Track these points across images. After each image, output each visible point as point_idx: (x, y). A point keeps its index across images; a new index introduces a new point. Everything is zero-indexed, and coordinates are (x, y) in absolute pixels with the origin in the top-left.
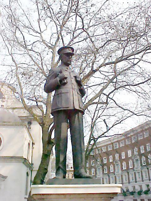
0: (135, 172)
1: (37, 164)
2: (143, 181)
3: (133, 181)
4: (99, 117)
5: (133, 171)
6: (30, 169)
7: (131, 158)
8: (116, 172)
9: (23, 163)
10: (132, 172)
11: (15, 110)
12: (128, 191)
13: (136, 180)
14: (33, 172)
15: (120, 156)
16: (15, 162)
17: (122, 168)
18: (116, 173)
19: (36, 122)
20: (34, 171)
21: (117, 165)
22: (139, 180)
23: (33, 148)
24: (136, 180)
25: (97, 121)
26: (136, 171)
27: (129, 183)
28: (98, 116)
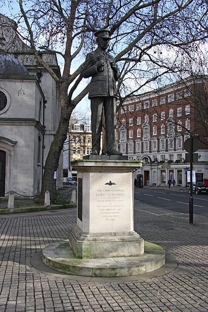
1: (125, 61)
2: (175, 150)
3: (180, 148)
4: (130, 70)
5: (164, 137)
6: (42, 133)
7: (140, 126)
8: (120, 141)
9: (35, 126)
10: (138, 142)
11: (20, 57)
12: (156, 160)
13: (142, 150)
14: (45, 136)
15: (151, 119)
17: (128, 136)
18: (120, 142)
19: (48, 74)
20: (47, 134)
21: (123, 132)
22: (178, 148)
23: (45, 107)
24: (142, 150)
25: (126, 76)
27: (158, 151)
28: (128, 70)
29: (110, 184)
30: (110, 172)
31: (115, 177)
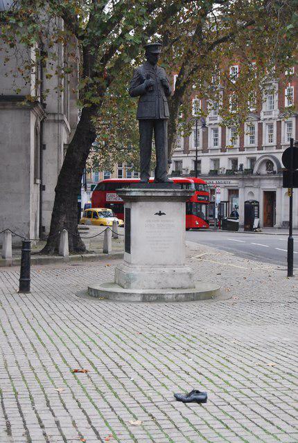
0: (261, 122)
16: (12, 109)
26: (265, 119)
29: (160, 214)
30: (151, 201)
31: (167, 207)
